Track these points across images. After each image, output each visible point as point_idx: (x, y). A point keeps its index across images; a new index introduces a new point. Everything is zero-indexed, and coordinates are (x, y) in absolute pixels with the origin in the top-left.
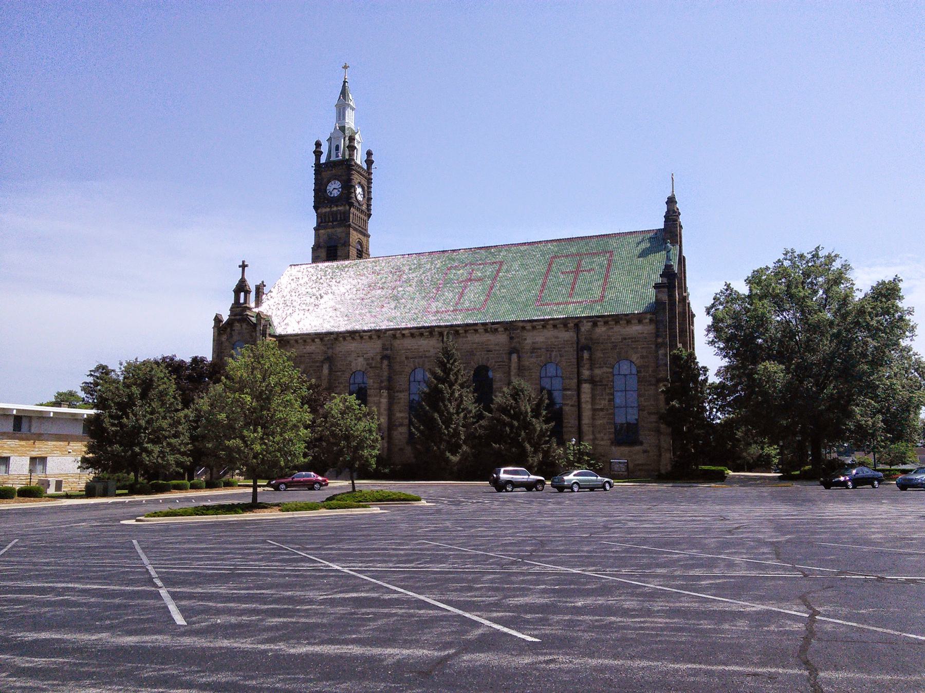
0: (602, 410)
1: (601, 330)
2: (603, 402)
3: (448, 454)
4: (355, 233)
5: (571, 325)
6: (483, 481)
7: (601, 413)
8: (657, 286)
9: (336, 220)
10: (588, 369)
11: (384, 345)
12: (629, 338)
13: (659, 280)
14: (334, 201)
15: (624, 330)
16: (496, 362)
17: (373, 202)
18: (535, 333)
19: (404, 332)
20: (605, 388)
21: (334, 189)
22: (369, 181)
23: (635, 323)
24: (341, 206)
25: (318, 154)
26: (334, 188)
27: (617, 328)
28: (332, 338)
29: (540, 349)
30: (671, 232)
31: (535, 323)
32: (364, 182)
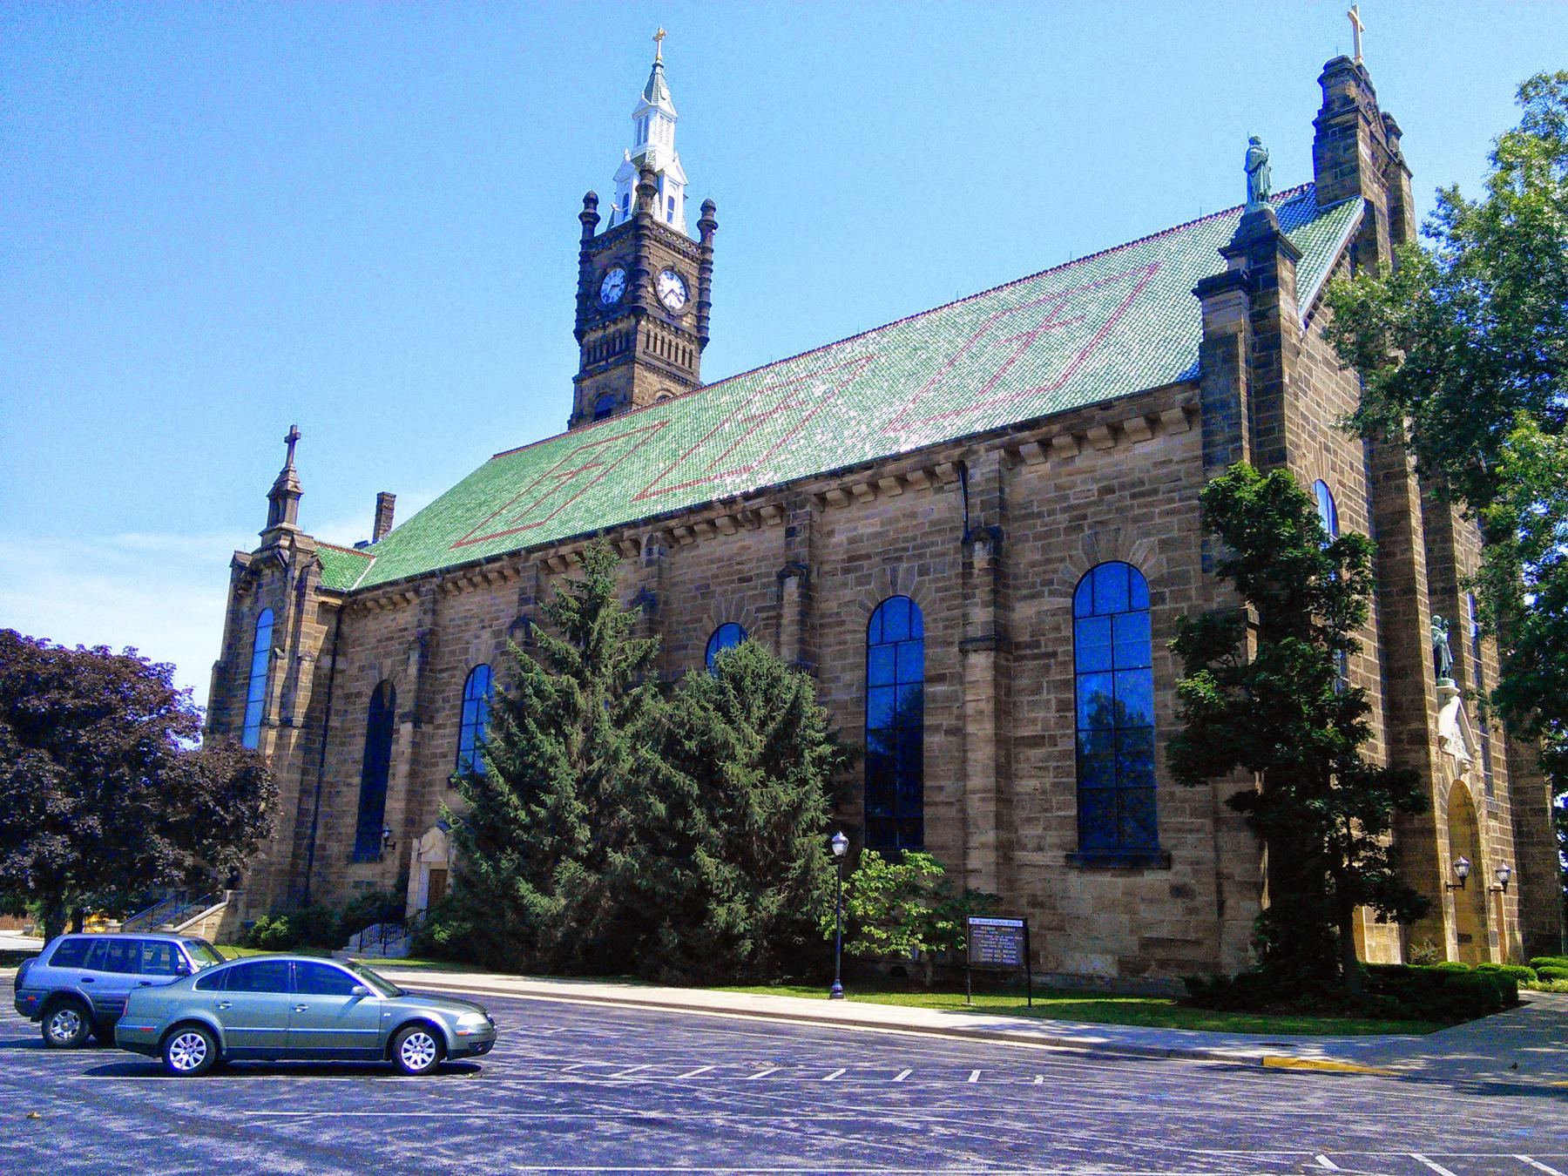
0: (1036, 741)
1: (1035, 473)
2: (1042, 714)
3: (524, 888)
4: (652, 378)
5: (945, 468)
6: (653, 980)
7: (1036, 753)
8: (1206, 289)
9: (614, 354)
10: (985, 605)
11: (522, 591)
12: (1123, 487)
13: (1221, 267)
14: (610, 313)
15: (1108, 460)
16: (759, 610)
17: (712, 313)
18: (854, 511)
19: (564, 550)
20: (1047, 668)
21: (614, 286)
22: (705, 266)
23: (1136, 431)
24: (621, 321)
25: (589, 220)
26: (613, 286)
27: (1085, 459)
28: (433, 586)
29: (868, 557)
30: (1338, 164)
31: (848, 479)
32: (691, 270)
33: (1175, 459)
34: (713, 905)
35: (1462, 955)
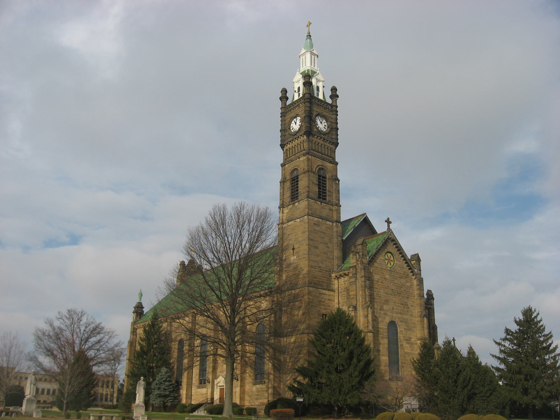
25: (284, 97)
33: (85, 388)
34: (311, 402)
35: (36, 415)
